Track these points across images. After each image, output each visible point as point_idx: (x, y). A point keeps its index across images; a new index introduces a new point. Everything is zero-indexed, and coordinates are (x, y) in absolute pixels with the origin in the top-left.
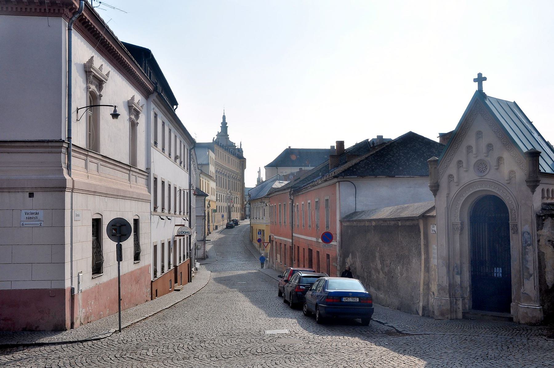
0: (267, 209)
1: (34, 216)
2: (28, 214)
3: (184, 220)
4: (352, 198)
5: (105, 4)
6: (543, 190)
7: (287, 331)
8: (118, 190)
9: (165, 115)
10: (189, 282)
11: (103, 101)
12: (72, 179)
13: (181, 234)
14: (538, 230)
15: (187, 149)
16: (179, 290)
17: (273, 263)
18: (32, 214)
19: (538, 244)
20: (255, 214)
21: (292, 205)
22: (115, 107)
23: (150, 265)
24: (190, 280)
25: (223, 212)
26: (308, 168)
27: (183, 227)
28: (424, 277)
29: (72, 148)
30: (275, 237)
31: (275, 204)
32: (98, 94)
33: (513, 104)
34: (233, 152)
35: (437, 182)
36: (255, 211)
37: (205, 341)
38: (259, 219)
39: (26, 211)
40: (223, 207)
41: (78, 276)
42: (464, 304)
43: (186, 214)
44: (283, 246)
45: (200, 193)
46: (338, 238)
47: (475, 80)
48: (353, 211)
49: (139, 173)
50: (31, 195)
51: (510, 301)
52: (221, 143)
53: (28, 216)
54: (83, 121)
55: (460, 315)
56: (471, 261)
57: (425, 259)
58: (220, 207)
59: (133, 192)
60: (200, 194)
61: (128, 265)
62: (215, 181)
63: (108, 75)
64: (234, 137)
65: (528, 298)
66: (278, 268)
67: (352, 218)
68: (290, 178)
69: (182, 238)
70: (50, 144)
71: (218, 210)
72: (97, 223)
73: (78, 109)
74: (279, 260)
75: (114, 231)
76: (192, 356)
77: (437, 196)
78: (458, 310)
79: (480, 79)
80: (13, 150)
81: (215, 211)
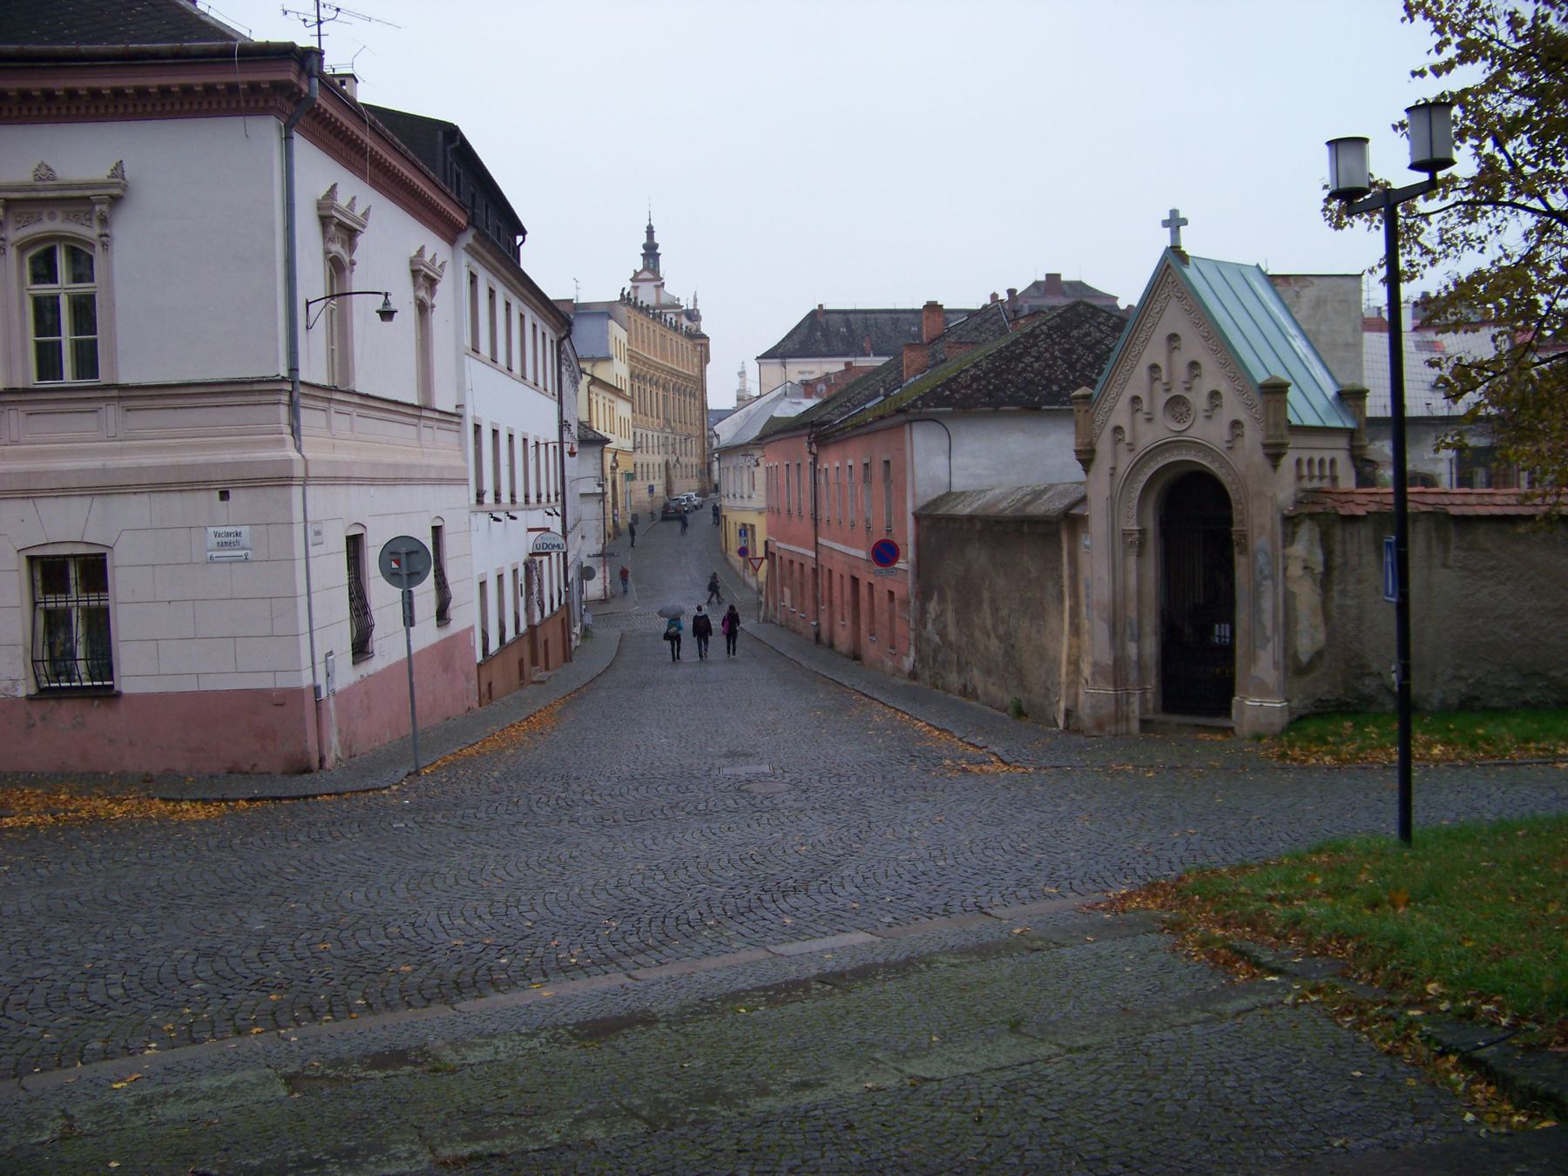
0: (760, 473)
1: (232, 539)
2: (220, 535)
3: (549, 514)
4: (941, 460)
5: (348, 13)
6: (1299, 462)
7: (766, 768)
8: (396, 466)
9: (495, 272)
10: (565, 661)
11: (357, 281)
12: (303, 456)
13: (541, 551)
14: (1284, 547)
15: (552, 341)
16: (542, 682)
17: (776, 609)
18: (228, 534)
19: (1284, 575)
20: (731, 485)
21: (815, 468)
22: (386, 294)
23: (472, 628)
24: (567, 657)
25: (651, 478)
26: (868, 359)
27: (548, 534)
28: (1070, 647)
29: (302, 390)
30: (778, 544)
31: (777, 464)
32: (347, 259)
33: (1255, 269)
34: (673, 322)
35: (1091, 444)
36: (731, 476)
37: (593, 791)
38: (742, 497)
39: (216, 529)
40: (651, 466)
41: (326, 661)
42: (1143, 702)
43: (553, 499)
44: (796, 566)
45: (591, 436)
46: (911, 554)
47: (1165, 224)
48: (942, 492)
49: (442, 421)
50: (224, 495)
51: (1233, 695)
52: (642, 302)
53: (220, 540)
54: (321, 326)
55: (1135, 726)
56: (1162, 612)
57: (1071, 607)
58: (645, 466)
59: (428, 467)
60: (592, 441)
61: (427, 633)
62: (630, 400)
63: (366, 214)
64: (678, 284)
65: (1263, 690)
66: (787, 620)
67: (937, 509)
68: (818, 389)
69: (545, 559)
70: (257, 387)
71: (639, 475)
72: (355, 544)
73: (308, 304)
74: (788, 603)
75: (394, 565)
76: (566, 818)
77: (1090, 473)
78: (1131, 715)
79: (1175, 222)
80: (179, 402)
81: (630, 477)
